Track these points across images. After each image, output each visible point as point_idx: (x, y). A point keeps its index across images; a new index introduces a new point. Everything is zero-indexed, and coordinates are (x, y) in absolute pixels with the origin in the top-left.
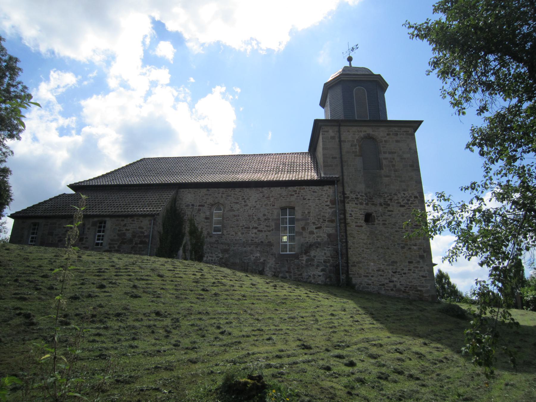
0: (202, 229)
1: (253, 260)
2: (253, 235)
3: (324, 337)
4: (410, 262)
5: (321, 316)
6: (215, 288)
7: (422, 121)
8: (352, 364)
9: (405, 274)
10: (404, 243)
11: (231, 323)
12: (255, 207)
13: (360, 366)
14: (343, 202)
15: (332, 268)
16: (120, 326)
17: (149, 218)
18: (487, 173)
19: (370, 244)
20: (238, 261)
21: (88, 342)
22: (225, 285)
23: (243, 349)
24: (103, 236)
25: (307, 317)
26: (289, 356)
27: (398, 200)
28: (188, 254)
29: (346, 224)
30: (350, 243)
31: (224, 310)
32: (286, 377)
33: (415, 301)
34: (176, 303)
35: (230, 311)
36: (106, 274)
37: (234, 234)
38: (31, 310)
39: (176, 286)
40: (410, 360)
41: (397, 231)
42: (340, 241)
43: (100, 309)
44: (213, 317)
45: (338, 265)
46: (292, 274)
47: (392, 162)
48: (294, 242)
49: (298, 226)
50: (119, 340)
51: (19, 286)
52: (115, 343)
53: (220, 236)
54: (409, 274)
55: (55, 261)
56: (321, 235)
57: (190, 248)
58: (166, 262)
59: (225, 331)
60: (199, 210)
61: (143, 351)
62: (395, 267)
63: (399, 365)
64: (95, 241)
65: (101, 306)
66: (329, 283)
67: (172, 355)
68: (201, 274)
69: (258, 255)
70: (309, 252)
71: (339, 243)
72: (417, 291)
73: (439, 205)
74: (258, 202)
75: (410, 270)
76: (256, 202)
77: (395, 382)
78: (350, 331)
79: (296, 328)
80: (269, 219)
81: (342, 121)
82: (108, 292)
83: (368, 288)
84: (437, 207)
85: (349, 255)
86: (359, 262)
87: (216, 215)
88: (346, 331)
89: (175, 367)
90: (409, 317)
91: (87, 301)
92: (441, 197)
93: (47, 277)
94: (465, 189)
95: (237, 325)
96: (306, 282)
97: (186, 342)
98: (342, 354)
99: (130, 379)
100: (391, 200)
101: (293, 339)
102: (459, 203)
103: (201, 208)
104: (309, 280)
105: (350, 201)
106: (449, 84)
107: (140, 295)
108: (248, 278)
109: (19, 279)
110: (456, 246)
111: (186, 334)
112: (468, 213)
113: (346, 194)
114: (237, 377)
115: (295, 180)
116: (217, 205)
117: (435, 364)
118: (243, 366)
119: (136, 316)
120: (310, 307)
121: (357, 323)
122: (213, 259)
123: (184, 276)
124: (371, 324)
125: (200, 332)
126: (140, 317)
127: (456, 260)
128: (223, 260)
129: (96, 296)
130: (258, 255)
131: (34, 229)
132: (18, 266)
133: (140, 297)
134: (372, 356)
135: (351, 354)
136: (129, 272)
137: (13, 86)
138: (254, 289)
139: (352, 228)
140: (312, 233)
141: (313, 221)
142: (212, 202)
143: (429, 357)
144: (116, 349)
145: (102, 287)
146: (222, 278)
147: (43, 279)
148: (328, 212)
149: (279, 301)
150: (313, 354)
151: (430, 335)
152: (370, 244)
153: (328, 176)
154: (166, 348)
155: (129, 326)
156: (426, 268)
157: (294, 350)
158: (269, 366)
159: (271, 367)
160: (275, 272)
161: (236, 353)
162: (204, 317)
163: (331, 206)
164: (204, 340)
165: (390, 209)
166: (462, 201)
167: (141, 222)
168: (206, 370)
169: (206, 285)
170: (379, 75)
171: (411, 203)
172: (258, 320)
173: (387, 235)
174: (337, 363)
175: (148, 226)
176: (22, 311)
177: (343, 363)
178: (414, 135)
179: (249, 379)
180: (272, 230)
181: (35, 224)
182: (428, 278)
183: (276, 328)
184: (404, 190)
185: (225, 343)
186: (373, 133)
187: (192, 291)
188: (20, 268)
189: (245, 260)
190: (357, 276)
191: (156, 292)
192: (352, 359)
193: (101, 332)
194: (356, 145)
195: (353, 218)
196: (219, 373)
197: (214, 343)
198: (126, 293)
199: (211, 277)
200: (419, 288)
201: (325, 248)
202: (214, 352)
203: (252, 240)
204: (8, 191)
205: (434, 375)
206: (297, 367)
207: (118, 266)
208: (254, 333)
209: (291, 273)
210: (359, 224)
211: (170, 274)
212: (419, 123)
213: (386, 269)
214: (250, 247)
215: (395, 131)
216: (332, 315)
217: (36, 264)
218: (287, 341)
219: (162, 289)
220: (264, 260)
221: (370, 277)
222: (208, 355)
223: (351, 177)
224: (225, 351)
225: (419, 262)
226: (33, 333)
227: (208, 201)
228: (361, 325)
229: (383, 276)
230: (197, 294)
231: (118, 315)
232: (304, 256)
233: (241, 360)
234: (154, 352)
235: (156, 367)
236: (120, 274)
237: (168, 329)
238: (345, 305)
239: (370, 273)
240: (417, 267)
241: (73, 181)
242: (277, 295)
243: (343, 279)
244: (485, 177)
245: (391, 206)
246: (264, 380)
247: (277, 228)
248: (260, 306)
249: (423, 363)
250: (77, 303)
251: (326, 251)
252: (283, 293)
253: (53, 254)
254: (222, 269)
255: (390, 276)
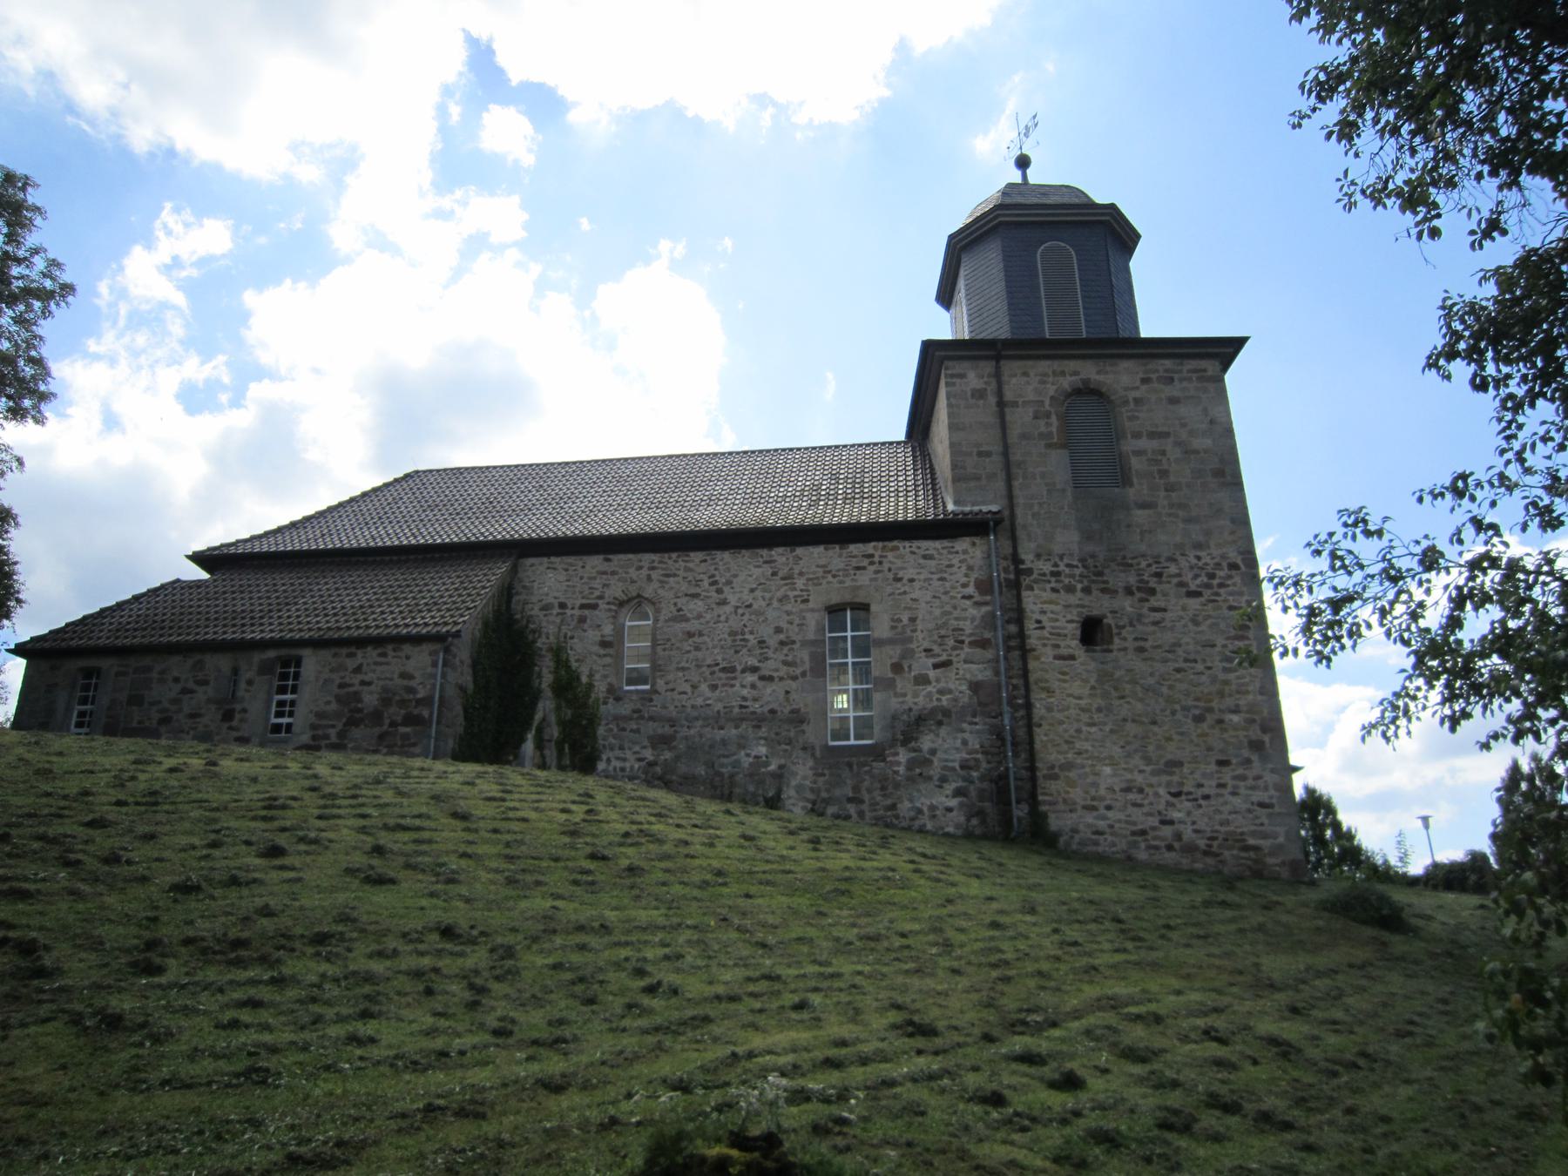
0: (591, 676)
1: (746, 765)
2: (745, 692)
3: (975, 997)
4: (1222, 763)
5: (961, 930)
6: (630, 851)
7: (1246, 339)
8: (1070, 1083)
9: (1206, 797)
10: (1202, 704)
11: (680, 957)
12: (749, 606)
13: (1096, 1084)
14: (1015, 586)
15: (985, 785)
16: (323, 976)
17: (427, 647)
18: (1508, 438)
19: (1099, 710)
20: (701, 770)
21: (216, 1027)
22: (661, 842)
23: (715, 1040)
24: (293, 703)
25: (917, 933)
26: (864, 1061)
27: (1179, 575)
28: (551, 753)
29: (1025, 652)
30: (1039, 710)
31: (657, 916)
32: (858, 1131)
33: (1241, 878)
34: (507, 898)
35: (675, 920)
36: (289, 813)
37: (689, 690)
38: (41, 928)
39: (508, 845)
40: (1255, 1062)
41: (1178, 670)
42: (1010, 703)
43: (265, 921)
44: (623, 939)
45: (1004, 777)
46: (865, 807)
47: (1158, 462)
48: (871, 709)
49: (880, 662)
50: (317, 1020)
51: (9, 855)
52: (302, 1028)
53: (647, 698)
54: (1221, 800)
55: (133, 778)
56: (952, 686)
57: (556, 734)
58: (479, 775)
59: (659, 983)
60: (582, 620)
61: (392, 1053)
62: (1176, 778)
63: (1223, 1082)
64: (268, 719)
65: (266, 912)
66: (978, 831)
67: (486, 1064)
68: (585, 808)
69: (763, 750)
70: (916, 739)
71: (1006, 708)
72: (1247, 848)
73: (1350, 552)
74: (758, 593)
75: (1222, 786)
76: (752, 590)
77: (1217, 1138)
78: (1055, 974)
79: (885, 970)
80: (793, 642)
81: (1006, 343)
82: (293, 869)
83: (1096, 843)
84: (1342, 559)
85: (1038, 746)
86: (1068, 766)
87: (636, 646)
88: (1040, 974)
89: (492, 1105)
90: (1233, 927)
91: (225, 898)
92: (1355, 524)
93: (105, 827)
94: (1435, 497)
95: (700, 962)
96: (908, 829)
97: (533, 1021)
98: (1035, 1050)
99: (338, 1153)
100: (1158, 575)
101: (875, 1004)
102: (1418, 542)
103: (586, 612)
104: (917, 823)
105: (1036, 581)
106: (1365, 157)
107: (392, 874)
108: (733, 819)
109: (13, 832)
110: (1404, 688)
111: (534, 996)
112: (1448, 573)
113: (1023, 562)
114: (691, 1140)
115: (867, 523)
116: (634, 602)
117: (1335, 1074)
118: (716, 1097)
119: (379, 943)
120: (926, 902)
121: (1073, 950)
122: (628, 765)
123: (533, 815)
124: (1117, 951)
125: (579, 989)
126: (391, 943)
127: (1409, 733)
128: (658, 769)
129: (255, 881)
130: (763, 750)
131: (86, 688)
132: (16, 793)
133: (392, 881)
134: (1132, 1055)
135: (1065, 1048)
136: (363, 805)
137: (19, 261)
138: (751, 853)
139: (1043, 663)
140: (922, 680)
141: (926, 645)
142: (619, 594)
143: (1313, 1053)
144: (305, 1048)
145: (275, 851)
146: (653, 819)
147: (90, 832)
148: (970, 616)
149: (828, 888)
150: (945, 1051)
151: (1304, 982)
152: (1099, 710)
153: (967, 509)
154: (468, 1041)
155: (354, 973)
156: (1270, 778)
157: (883, 1040)
158: (799, 1096)
159: (808, 1100)
160: (814, 803)
161: (696, 1055)
162: (593, 941)
163: (978, 598)
164: (593, 1012)
165: (1156, 604)
166: (1426, 537)
167: (408, 658)
168: (594, 1115)
169: (605, 840)
170: (1113, 207)
171: (1221, 585)
172: (764, 945)
173: (1151, 681)
174: (1024, 1080)
175: (429, 670)
176: (11, 934)
177: (1041, 1079)
178: (1223, 380)
179: (733, 1145)
180: (804, 674)
181: (89, 673)
182: (1277, 809)
183: (822, 969)
184: (1198, 546)
185: (658, 1020)
186: (1101, 378)
187: (556, 860)
188: (16, 801)
189: (722, 765)
190: (1061, 807)
191: (443, 865)
192: (1069, 1065)
193: (264, 993)
194: (1048, 415)
195: (1045, 633)
196: (639, 1124)
197: (626, 1022)
198: (350, 871)
199: (615, 817)
200: (1251, 842)
201: (965, 725)
202: (621, 1052)
203: (741, 707)
204: (9, 575)
205: (1337, 1113)
206: (895, 1097)
207: (328, 789)
208: (751, 988)
209: (862, 802)
210: (1064, 651)
211: (489, 810)
212: (1237, 344)
213: (1151, 786)
214: (737, 727)
215: (1166, 371)
216: (995, 925)
217: (73, 786)
218: (857, 1011)
219: (464, 855)
220: (781, 767)
221: (1103, 811)
222: (603, 1063)
223: (1036, 508)
224: (659, 1047)
225: (1248, 761)
226: (40, 1002)
227: (609, 593)
228: (1089, 954)
229: (1140, 805)
230: (572, 871)
231: (321, 939)
232: (901, 750)
233: (713, 1077)
234: (428, 1056)
235: (430, 1108)
236: (335, 811)
237: (478, 981)
238: (1036, 896)
239: (1102, 799)
240: (1243, 778)
241: (200, 546)
242: (823, 870)
243: (1019, 819)
244: (1503, 452)
245: (1159, 596)
246: (787, 1145)
247: (818, 669)
248: (771, 904)
249: (1296, 1074)
250: (192, 903)
251: (967, 736)
252: (840, 861)
253: (131, 757)
254: (653, 793)
255: (1161, 807)
